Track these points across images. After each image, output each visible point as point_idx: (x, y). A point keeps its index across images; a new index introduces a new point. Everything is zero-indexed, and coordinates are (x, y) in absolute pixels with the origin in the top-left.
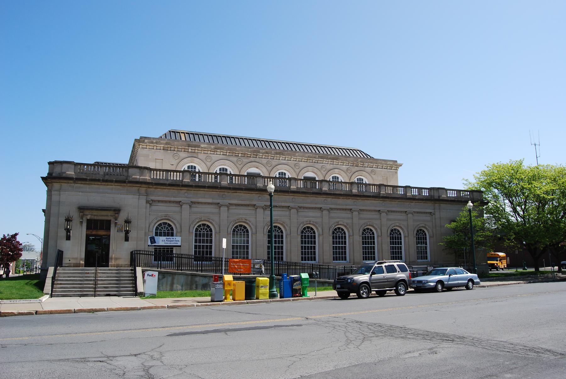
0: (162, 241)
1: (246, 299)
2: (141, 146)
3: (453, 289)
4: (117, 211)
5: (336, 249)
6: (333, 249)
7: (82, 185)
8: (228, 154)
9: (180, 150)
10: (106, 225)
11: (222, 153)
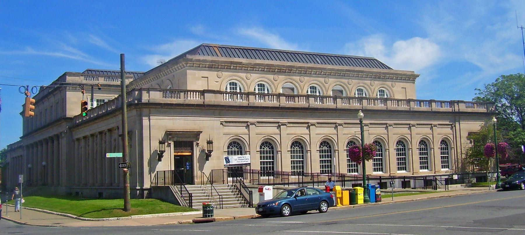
0: (235, 160)
1: (350, 204)
2: (188, 65)
3: (309, 212)
4: (197, 135)
5: (264, 165)
6: (261, 165)
7: (167, 110)
8: (265, 70)
9: (223, 67)
10: (189, 145)
11: (260, 69)
